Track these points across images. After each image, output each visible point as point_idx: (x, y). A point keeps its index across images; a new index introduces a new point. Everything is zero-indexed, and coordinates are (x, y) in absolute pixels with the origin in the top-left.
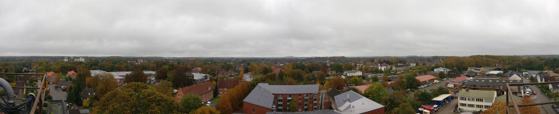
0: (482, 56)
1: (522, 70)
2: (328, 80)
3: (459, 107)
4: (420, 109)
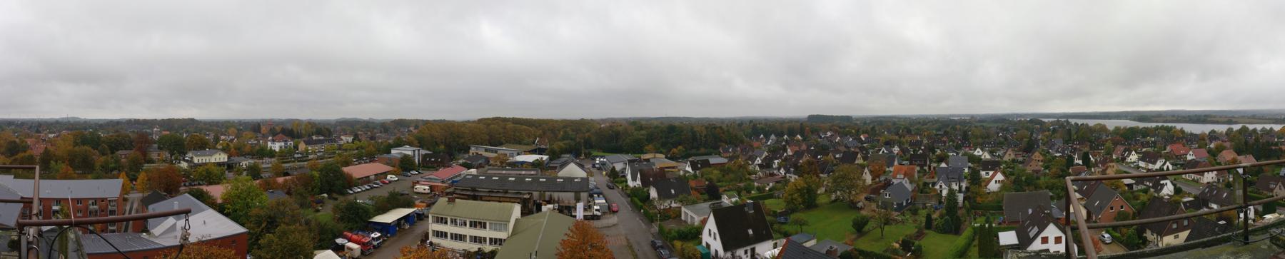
0: (505, 120)
1: (595, 153)
2: (147, 171)
3: (432, 239)
4: (339, 241)
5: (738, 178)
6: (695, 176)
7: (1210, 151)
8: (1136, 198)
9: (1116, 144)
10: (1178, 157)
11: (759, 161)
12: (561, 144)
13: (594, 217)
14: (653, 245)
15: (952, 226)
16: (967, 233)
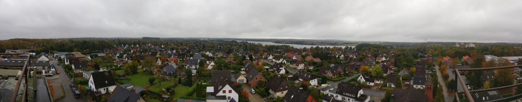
0: (19, 39)
5: (108, 61)
6: (92, 61)
7: (302, 56)
8: (269, 75)
9: (264, 51)
10: (290, 58)
11: (118, 55)
12: (41, 48)
13: (50, 76)
14: (71, 86)
15: (189, 83)
16: (194, 86)
